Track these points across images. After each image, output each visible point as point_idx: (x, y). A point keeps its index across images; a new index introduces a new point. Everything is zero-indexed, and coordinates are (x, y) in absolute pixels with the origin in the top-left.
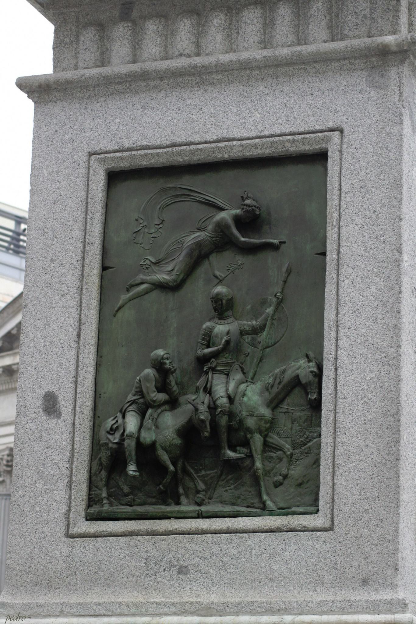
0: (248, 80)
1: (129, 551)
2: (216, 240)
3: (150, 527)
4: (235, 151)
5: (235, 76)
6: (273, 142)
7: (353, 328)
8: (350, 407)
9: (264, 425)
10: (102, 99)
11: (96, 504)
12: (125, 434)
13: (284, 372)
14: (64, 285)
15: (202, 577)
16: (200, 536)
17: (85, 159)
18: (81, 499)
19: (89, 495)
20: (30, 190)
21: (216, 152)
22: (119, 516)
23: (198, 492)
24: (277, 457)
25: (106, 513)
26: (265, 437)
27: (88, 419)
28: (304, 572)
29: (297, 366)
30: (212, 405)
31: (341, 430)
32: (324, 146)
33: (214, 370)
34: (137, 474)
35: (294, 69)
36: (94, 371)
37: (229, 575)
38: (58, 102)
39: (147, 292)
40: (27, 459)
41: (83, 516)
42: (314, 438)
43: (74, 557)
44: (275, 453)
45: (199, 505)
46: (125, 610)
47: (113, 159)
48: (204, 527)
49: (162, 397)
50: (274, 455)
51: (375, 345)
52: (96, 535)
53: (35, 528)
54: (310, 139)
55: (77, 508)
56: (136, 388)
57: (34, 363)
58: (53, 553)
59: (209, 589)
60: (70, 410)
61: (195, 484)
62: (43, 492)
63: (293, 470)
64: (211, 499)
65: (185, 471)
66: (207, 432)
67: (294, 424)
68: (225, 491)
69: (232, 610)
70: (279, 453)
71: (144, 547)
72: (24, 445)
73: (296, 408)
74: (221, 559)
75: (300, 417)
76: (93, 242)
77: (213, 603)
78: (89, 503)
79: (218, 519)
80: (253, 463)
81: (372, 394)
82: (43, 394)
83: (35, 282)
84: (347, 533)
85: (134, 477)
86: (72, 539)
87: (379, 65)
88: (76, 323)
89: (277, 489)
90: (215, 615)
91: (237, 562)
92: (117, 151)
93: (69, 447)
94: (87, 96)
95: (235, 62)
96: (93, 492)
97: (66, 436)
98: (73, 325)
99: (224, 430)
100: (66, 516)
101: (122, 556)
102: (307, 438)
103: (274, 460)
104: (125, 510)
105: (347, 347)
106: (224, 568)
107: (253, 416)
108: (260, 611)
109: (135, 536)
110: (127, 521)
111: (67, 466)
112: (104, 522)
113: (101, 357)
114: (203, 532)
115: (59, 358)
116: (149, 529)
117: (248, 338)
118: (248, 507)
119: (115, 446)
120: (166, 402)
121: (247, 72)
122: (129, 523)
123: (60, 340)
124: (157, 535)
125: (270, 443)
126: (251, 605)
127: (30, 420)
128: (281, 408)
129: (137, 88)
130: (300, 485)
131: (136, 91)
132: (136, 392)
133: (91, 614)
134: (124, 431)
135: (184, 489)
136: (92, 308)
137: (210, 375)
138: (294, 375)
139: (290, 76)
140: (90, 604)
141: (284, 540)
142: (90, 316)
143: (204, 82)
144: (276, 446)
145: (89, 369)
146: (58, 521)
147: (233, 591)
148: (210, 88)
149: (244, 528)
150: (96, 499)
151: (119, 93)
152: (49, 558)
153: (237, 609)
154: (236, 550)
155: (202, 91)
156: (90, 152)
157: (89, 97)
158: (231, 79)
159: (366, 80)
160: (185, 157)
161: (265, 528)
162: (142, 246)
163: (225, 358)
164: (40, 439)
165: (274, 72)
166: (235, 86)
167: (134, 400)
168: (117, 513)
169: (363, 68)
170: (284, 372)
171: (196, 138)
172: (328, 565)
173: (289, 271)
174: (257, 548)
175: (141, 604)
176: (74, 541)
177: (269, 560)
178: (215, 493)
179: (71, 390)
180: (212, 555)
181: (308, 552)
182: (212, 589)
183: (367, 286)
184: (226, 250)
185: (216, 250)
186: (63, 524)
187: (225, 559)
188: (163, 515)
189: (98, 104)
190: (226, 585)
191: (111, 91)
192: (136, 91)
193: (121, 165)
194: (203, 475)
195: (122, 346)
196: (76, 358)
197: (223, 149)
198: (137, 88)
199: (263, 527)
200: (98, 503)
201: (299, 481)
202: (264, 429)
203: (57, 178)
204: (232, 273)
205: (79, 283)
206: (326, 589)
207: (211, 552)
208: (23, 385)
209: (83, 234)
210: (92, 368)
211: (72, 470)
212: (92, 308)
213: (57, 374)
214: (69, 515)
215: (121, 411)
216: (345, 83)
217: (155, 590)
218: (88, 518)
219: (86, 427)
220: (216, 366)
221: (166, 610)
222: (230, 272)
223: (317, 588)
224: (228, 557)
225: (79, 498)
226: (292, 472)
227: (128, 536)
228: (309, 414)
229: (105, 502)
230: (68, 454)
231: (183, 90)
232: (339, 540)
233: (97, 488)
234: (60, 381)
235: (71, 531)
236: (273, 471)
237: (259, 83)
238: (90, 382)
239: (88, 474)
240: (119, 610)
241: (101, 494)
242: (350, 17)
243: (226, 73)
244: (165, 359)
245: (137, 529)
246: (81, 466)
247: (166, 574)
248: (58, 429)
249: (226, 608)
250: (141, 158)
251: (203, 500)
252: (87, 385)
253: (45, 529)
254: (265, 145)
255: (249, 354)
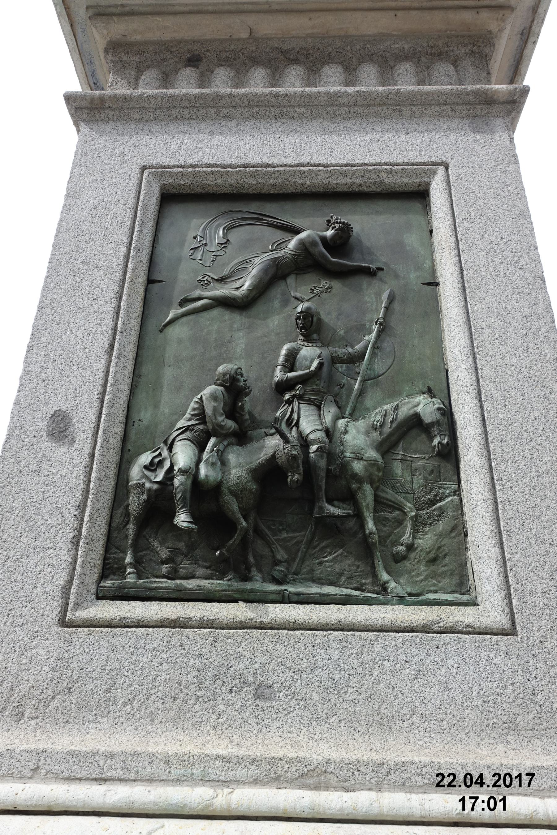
0: (333, 118)
1: (168, 653)
2: (298, 259)
3: (206, 614)
4: (319, 177)
5: (320, 112)
6: (367, 170)
7: (497, 357)
8: (511, 453)
9: (376, 473)
10: (163, 123)
11: (114, 574)
12: (176, 468)
13: (397, 408)
14: (97, 289)
15: (297, 707)
16: (292, 632)
17: (138, 171)
18: (92, 564)
19: (105, 559)
20: (66, 195)
21: (297, 177)
22: (153, 594)
23: (277, 563)
24: (395, 518)
25: (131, 588)
26: (376, 489)
27: (115, 451)
28: (480, 706)
29: (415, 403)
30: (303, 443)
31: (503, 483)
32: (426, 180)
33: (300, 398)
34: (194, 526)
35: (387, 109)
36: (128, 391)
37: (345, 705)
38: (110, 122)
39: (204, 309)
40: (12, 499)
41: (92, 592)
42: (446, 497)
43: (70, 660)
44: (391, 513)
45: (279, 582)
46: (161, 770)
47: (172, 174)
48: (298, 618)
49: (231, 424)
50: (389, 516)
51: (533, 378)
52: (113, 624)
53: (8, 608)
54: (412, 170)
55: (84, 578)
56: (194, 409)
57: (43, 374)
58: (34, 651)
59: (311, 730)
60: (90, 435)
61: (272, 551)
62: (32, 550)
63: (420, 538)
64: (297, 575)
65: (257, 531)
66: (299, 474)
67: (414, 475)
68: (318, 564)
69: (368, 778)
70: (396, 513)
71: (196, 649)
72: (11, 481)
73: (415, 455)
74: (331, 675)
75: (424, 467)
76: (141, 249)
77: (329, 762)
78: (103, 572)
79: (318, 606)
80: (362, 525)
81: (541, 438)
82: (51, 413)
83: (59, 284)
84: (542, 640)
85: (188, 531)
86: (71, 629)
87: (483, 114)
88: (110, 331)
89: (398, 564)
90: (335, 788)
91: (359, 682)
92: (178, 167)
93: (82, 486)
94: (145, 119)
95: (324, 94)
96: (112, 556)
97: (79, 471)
98: (105, 333)
99: (323, 474)
100: (64, 590)
101: (155, 662)
102: (436, 495)
103: (391, 523)
104: (164, 585)
105: (493, 378)
106: (336, 692)
107: (362, 459)
108: (421, 783)
109: (178, 627)
110: (165, 603)
111: (76, 513)
112: (127, 602)
113: (139, 376)
114: (296, 626)
115: (80, 369)
116: (205, 618)
117: (342, 368)
118: (356, 589)
119: (155, 487)
120: (234, 434)
121: (334, 108)
122: (169, 606)
123: (85, 348)
124: (216, 628)
125: (384, 498)
126: (403, 769)
127: (26, 445)
128: (394, 453)
129: (206, 115)
130: (433, 561)
131: (203, 119)
132: (193, 415)
133: (94, 776)
134: (172, 466)
135: (254, 557)
136: (133, 317)
137: (296, 405)
138: (411, 412)
139: (382, 118)
140: (94, 754)
141: (437, 648)
142: (130, 325)
143: (282, 116)
144: (392, 504)
145: (122, 387)
146: (49, 598)
147: (357, 736)
148: (289, 122)
149: (368, 623)
150: (116, 566)
151: (183, 118)
152: (24, 661)
153: (377, 777)
154: (355, 661)
155: (280, 123)
156: (144, 166)
157: (148, 120)
158: (314, 115)
159: (469, 126)
160: (259, 180)
161: (402, 625)
162: (201, 262)
163: (316, 385)
164: (38, 472)
165: (365, 111)
166: (319, 122)
167: (189, 426)
168: (150, 589)
169: (464, 116)
170: (397, 408)
171: (276, 161)
172: (521, 695)
173: (392, 299)
174: (391, 658)
175: (191, 758)
176: (75, 633)
177: (416, 681)
178: (303, 566)
179: (94, 410)
180: (314, 667)
181: (481, 669)
182: (318, 730)
183: (508, 312)
184: (308, 273)
185: (295, 272)
186: (56, 604)
187: (337, 676)
188: (226, 595)
189: (158, 127)
190: (343, 723)
191: (174, 116)
192: (203, 119)
193: (181, 182)
194: (285, 538)
195: (170, 366)
196: (105, 371)
197: (306, 174)
198: (206, 115)
199: (399, 623)
200: (117, 573)
201: (432, 555)
202: (376, 479)
203: (101, 186)
204: (317, 296)
205: (118, 288)
206: (526, 740)
207: (312, 662)
208: (22, 400)
209: (129, 239)
210: (126, 387)
211: (82, 520)
212: (133, 317)
213: (76, 389)
214: (70, 589)
215: (165, 442)
216: (446, 127)
217: (214, 727)
218: (100, 595)
219: (111, 460)
220: (303, 394)
221: (240, 773)
222: (314, 295)
223: (509, 738)
224: (342, 672)
225: (90, 563)
226: (419, 542)
227: (167, 627)
228: (436, 463)
229: (129, 570)
230: (78, 495)
231: (257, 121)
232: (533, 652)
233: (117, 548)
234: (77, 398)
235: (69, 616)
236: (390, 538)
237: (346, 121)
238: (122, 403)
239: (107, 528)
240: (149, 769)
241: (125, 559)
242: (443, 78)
243: (310, 108)
244: (239, 375)
245: (185, 616)
246: (97, 515)
247: (233, 698)
248: (69, 459)
249: (356, 773)
250: (206, 176)
251: (286, 575)
252: (118, 406)
253: (25, 611)
254: (356, 173)
255: (344, 385)
